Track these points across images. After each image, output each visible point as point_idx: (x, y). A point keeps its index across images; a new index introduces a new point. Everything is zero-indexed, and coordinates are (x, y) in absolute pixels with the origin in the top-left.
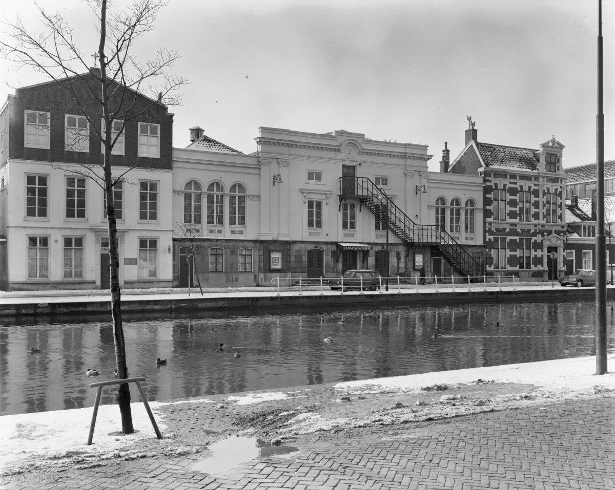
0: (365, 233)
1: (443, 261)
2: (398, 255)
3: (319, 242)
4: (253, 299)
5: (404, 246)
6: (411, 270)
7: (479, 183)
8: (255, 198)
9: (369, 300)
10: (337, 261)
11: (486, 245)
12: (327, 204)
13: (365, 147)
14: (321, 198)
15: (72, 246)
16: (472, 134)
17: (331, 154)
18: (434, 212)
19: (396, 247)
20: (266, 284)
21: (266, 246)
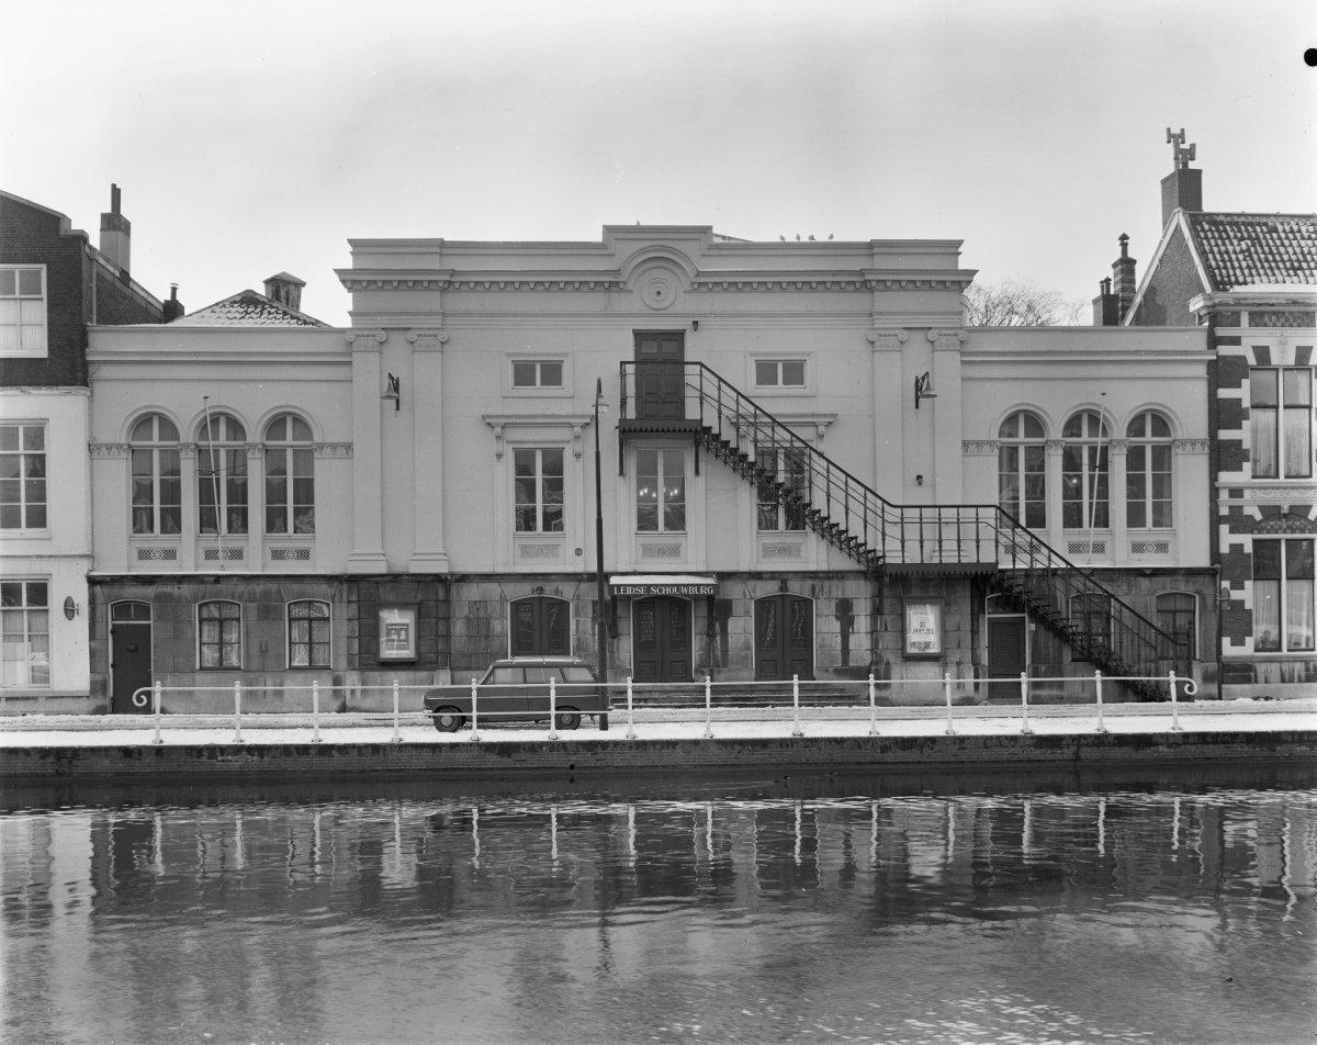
0: (722, 534)
1: (1030, 627)
2: (845, 611)
3: (546, 576)
4: (59, 753)
5: (866, 579)
6: (890, 656)
8: (341, 451)
9: (492, 760)
10: (615, 635)
11: (1221, 566)
12: (578, 456)
13: (708, 266)
14: (558, 438)
15: (21, 605)
16: (1185, 186)
18: (990, 465)
19: (835, 582)
20: (368, 703)
21: (367, 592)
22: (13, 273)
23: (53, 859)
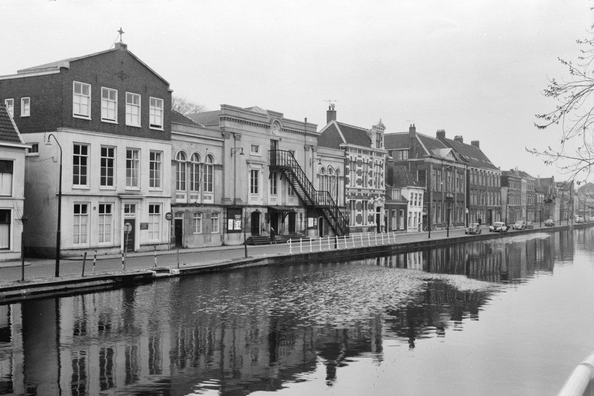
7: (342, 156)
12: (262, 173)
16: (331, 114)
17: (263, 130)
22: (155, 101)
23: (23, 373)
